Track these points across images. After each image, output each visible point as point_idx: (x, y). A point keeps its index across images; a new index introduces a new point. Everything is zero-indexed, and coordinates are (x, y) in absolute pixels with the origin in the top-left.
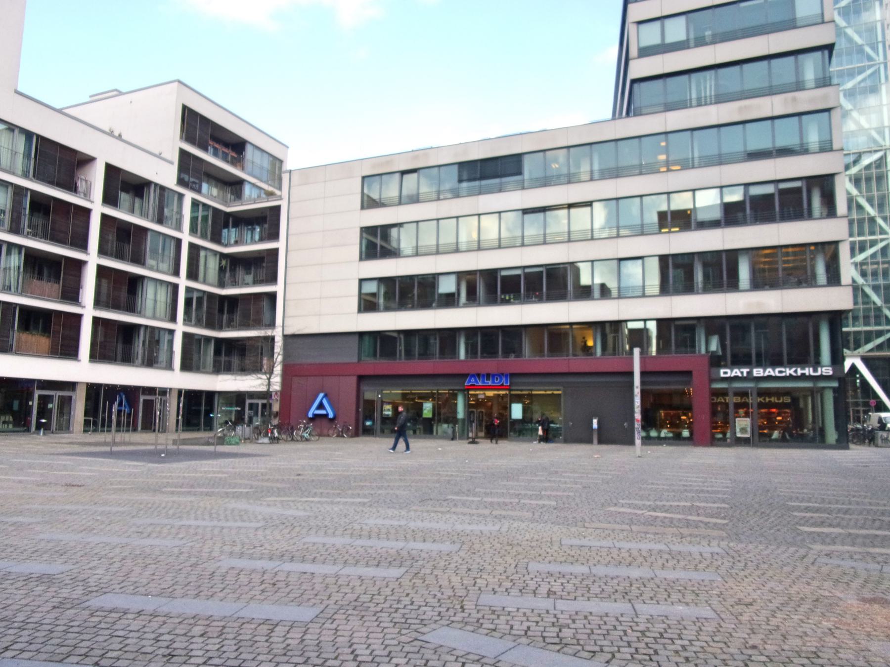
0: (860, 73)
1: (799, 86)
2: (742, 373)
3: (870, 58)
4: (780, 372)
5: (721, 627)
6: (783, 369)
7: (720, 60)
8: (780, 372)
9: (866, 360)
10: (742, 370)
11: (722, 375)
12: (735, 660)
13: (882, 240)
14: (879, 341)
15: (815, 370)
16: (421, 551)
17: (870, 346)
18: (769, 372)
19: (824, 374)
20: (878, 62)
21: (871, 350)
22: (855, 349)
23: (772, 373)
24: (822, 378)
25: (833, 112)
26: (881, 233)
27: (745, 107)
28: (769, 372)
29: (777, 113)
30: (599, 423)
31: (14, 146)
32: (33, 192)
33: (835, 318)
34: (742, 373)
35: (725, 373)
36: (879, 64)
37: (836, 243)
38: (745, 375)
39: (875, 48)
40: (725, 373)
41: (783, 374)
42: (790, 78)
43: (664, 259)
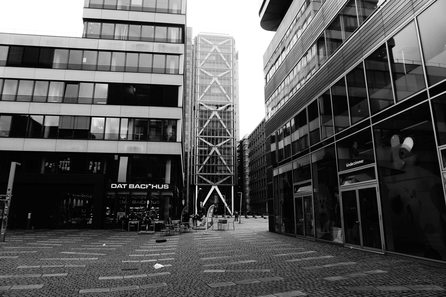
1: (167, 41)
2: (123, 186)
3: (228, 67)
4: (143, 186)
5: (196, 292)
6: (145, 185)
7: (130, 19)
8: (143, 186)
9: (219, 187)
10: (123, 185)
11: (112, 187)
13: (228, 138)
14: (225, 179)
15: (160, 186)
17: (221, 181)
18: (138, 186)
21: (221, 183)
22: (216, 182)
25: (181, 56)
28: (138, 186)
29: (155, 51)
30: (31, 216)
34: (123, 186)
35: (114, 186)
37: (176, 120)
38: (124, 187)
39: (230, 64)
40: (114, 186)
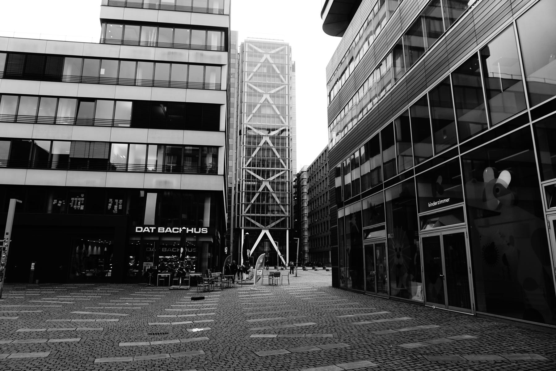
0: (277, 87)
1: (207, 48)
2: (150, 230)
3: (282, 81)
4: (175, 230)
6: (178, 229)
7: (160, 21)
8: (175, 230)
9: (270, 231)
13: (282, 171)
15: (197, 230)
16: (38, 352)
17: (273, 224)
18: (169, 230)
19: (202, 232)
21: (274, 227)
22: (267, 225)
23: (170, 231)
25: (223, 67)
26: (282, 168)
27: (173, 53)
28: (169, 230)
31: (87, 149)
34: (150, 230)
36: (286, 84)
37: (217, 147)
38: (152, 231)
41: (178, 232)
43: (231, 187)
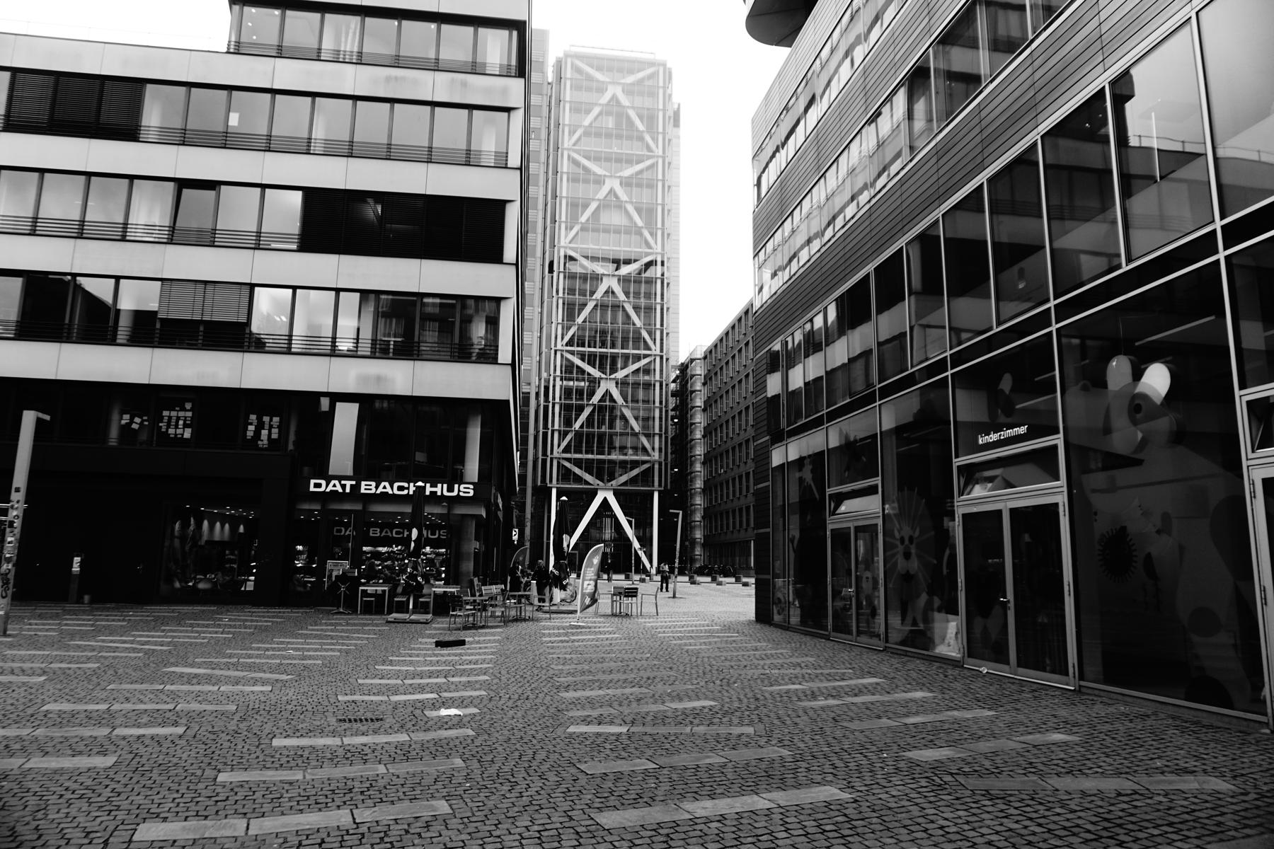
0: (638, 162)
1: (475, 68)
2: (344, 487)
8: (400, 488)
9: (617, 494)
12: (572, 828)
13: (646, 356)
15: (450, 489)
18: (385, 487)
19: (461, 494)
20: (656, 154)
21: (625, 484)
22: (609, 481)
24: (459, 500)
25: (513, 114)
28: (385, 487)
31: (199, 299)
32: (1003, 565)
33: (493, 411)
34: (344, 487)
35: (318, 485)
37: (498, 300)
38: (348, 490)
40: (318, 485)
41: (405, 492)
42: (463, 55)
43: (529, 393)
